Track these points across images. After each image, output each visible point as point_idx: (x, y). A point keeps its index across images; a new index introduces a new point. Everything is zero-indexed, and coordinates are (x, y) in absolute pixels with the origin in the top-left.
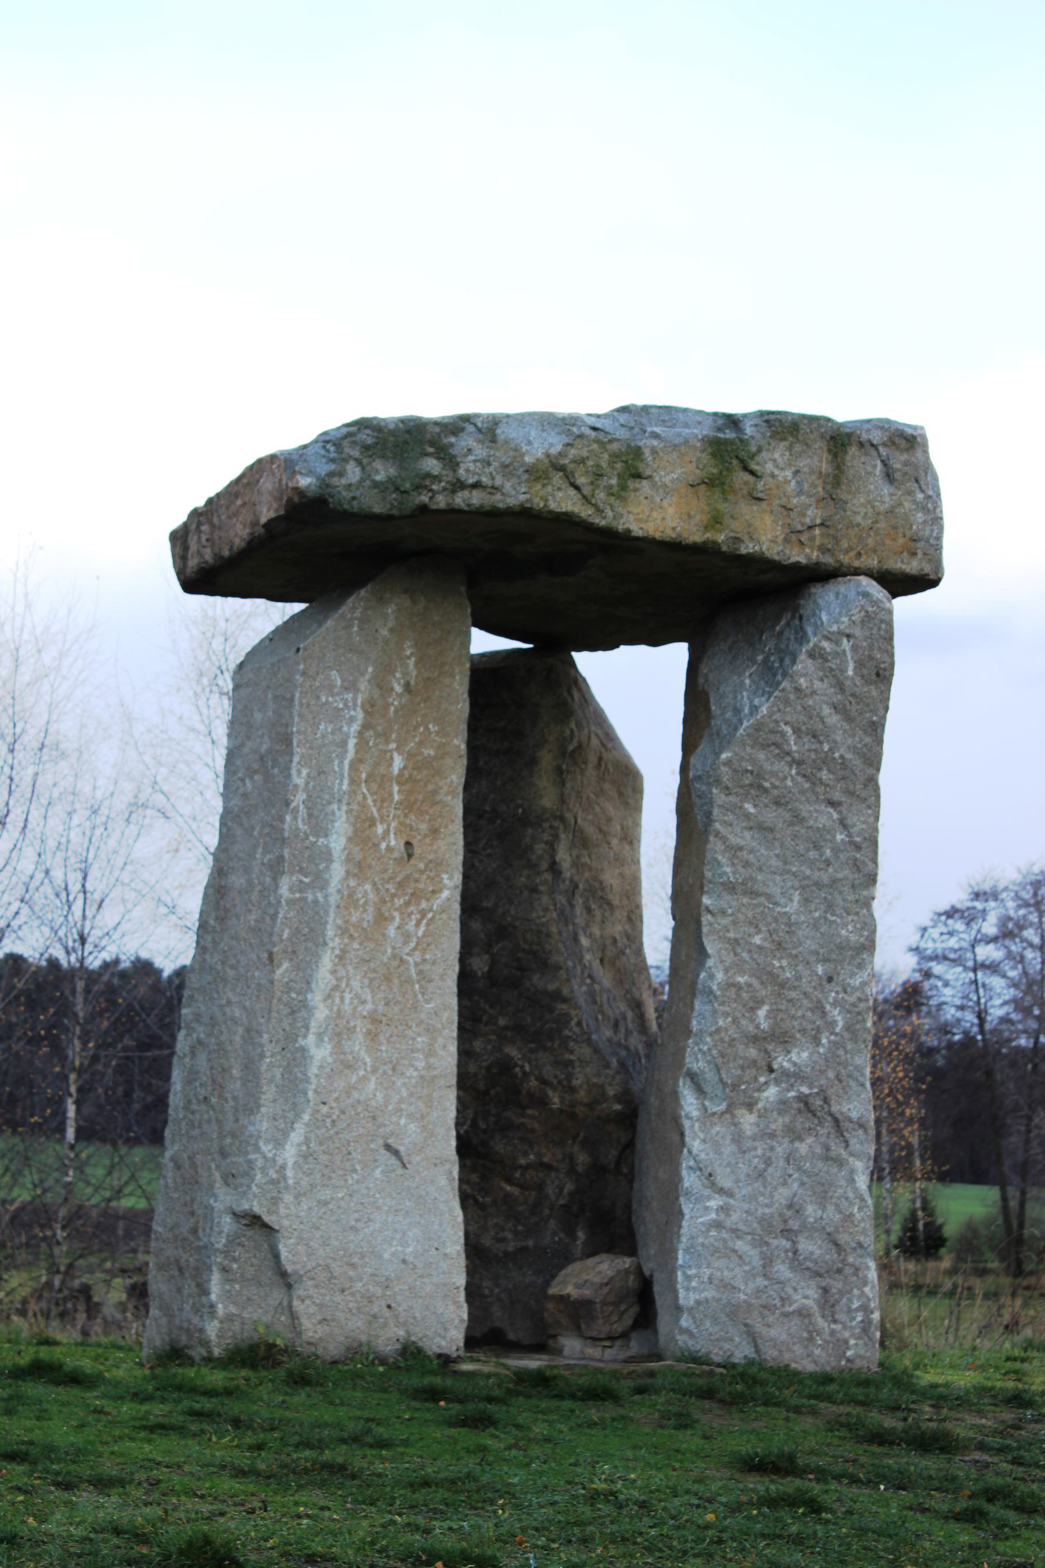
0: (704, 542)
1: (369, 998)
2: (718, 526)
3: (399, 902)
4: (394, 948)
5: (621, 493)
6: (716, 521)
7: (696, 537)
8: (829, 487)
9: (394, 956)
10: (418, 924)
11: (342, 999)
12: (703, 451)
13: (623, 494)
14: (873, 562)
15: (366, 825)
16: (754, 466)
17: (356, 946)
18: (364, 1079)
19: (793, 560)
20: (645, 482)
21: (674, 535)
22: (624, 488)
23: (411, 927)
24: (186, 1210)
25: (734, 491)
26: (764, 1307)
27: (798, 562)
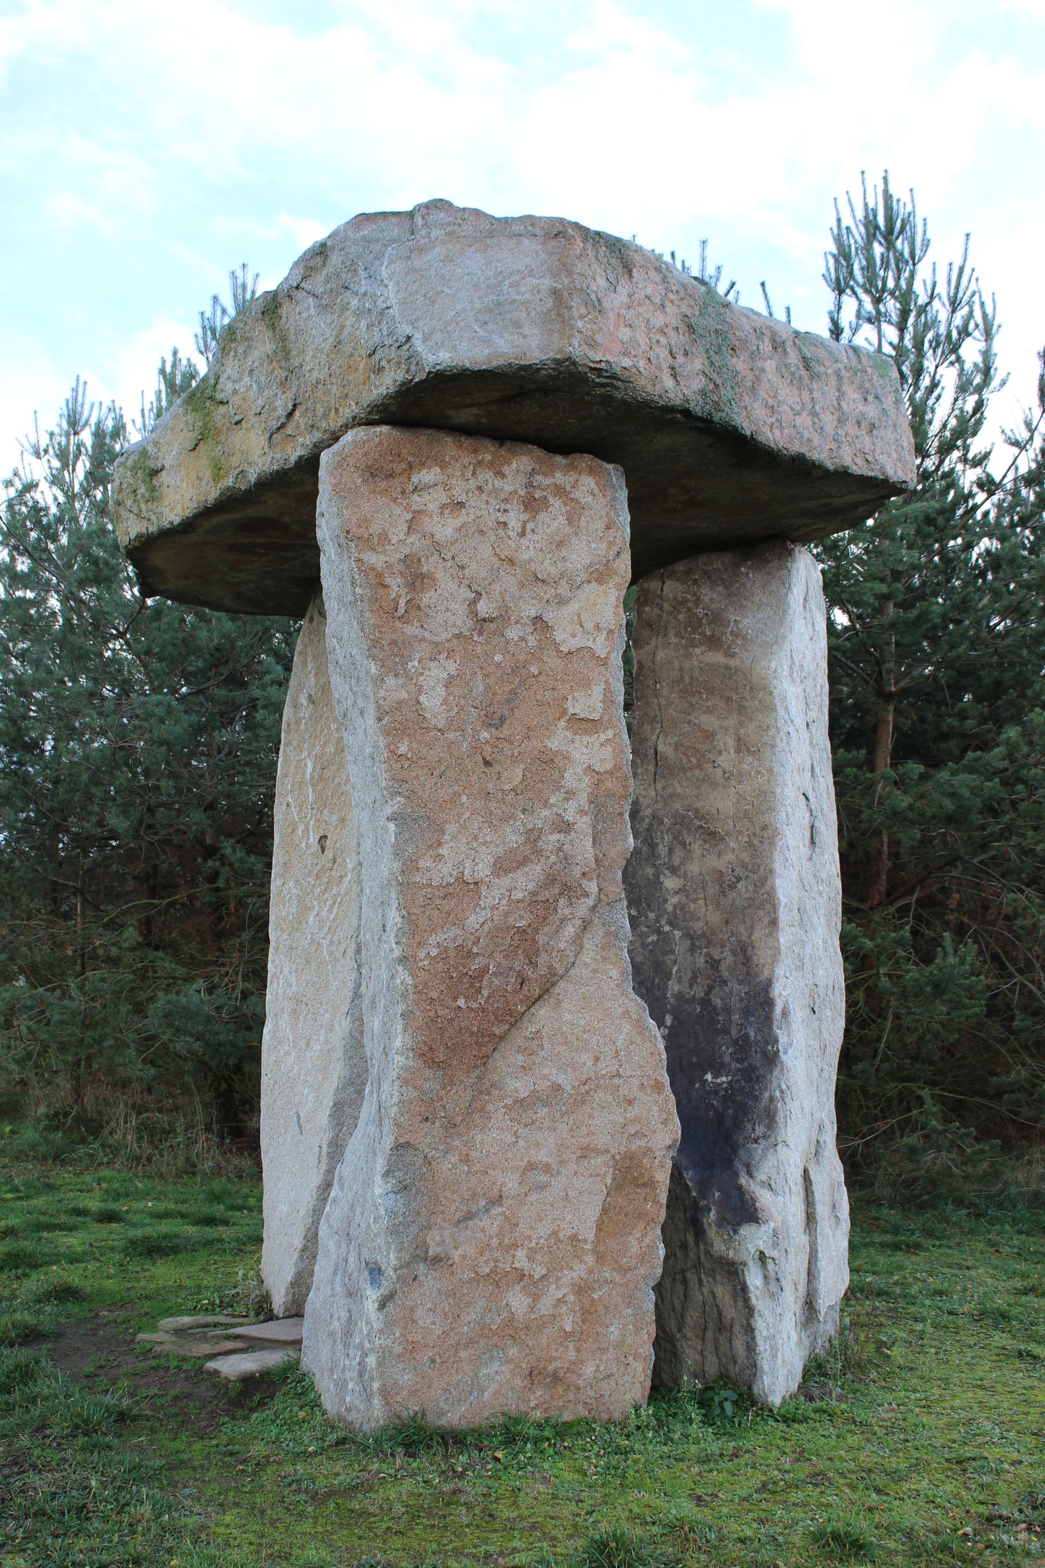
0: (222, 494)
1: (294, 983)
2: (222, 472)
3: (317, 891)
4: (312, 934)
5: (154, 495)
6: (218, 470)
7: (213, 495)
8: (283, 364)
9: (313, 941)
10: (330, 910)
11: (278, 983)
12: (186, 414)
13: (156, 494)
14: (349, 410)
15: (289, 830)
16: (220, 396)
17: (285, 937)
18: (287, 1054)
19: (293, 459)
20: (163, 473)
21: (196, 505)
22: (153, 489)
23: (324, 914)
24: (50, 1161)
25: (219, 432)
26: (912, 1369)
27: (301, 457)
